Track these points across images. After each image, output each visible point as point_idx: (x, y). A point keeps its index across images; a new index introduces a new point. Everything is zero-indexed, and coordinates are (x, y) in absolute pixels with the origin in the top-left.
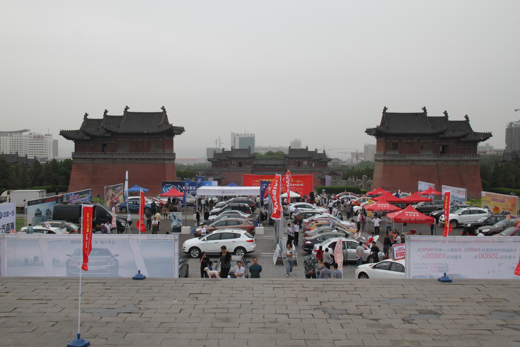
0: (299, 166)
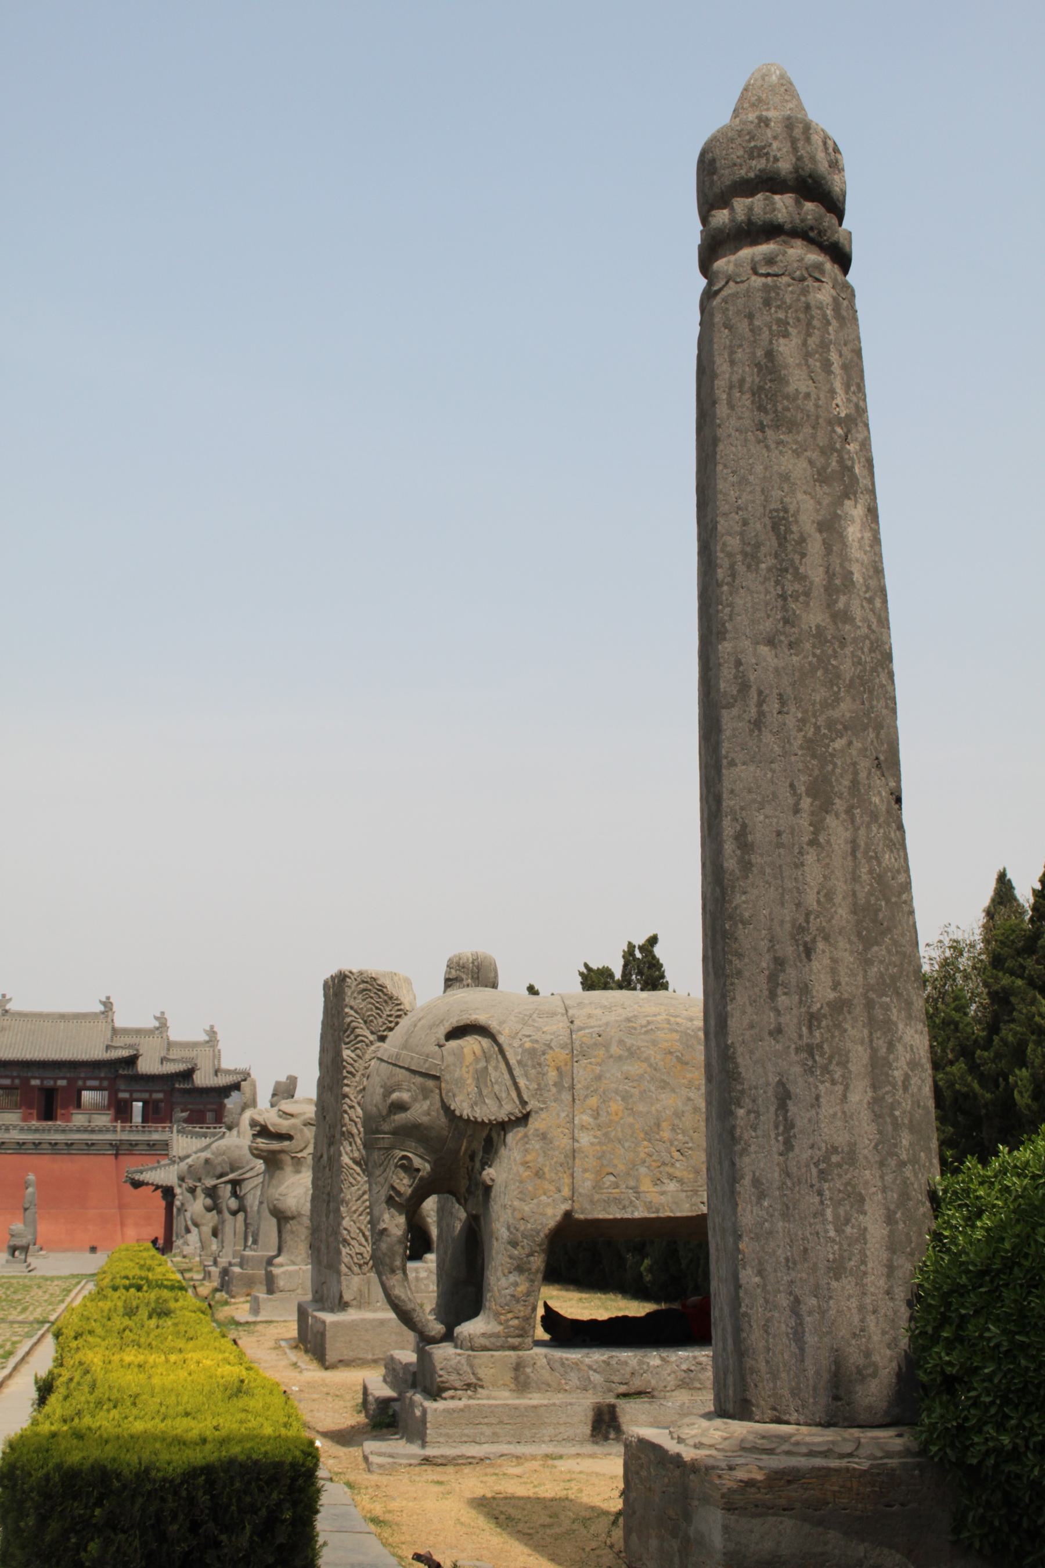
0: (48, 1114)
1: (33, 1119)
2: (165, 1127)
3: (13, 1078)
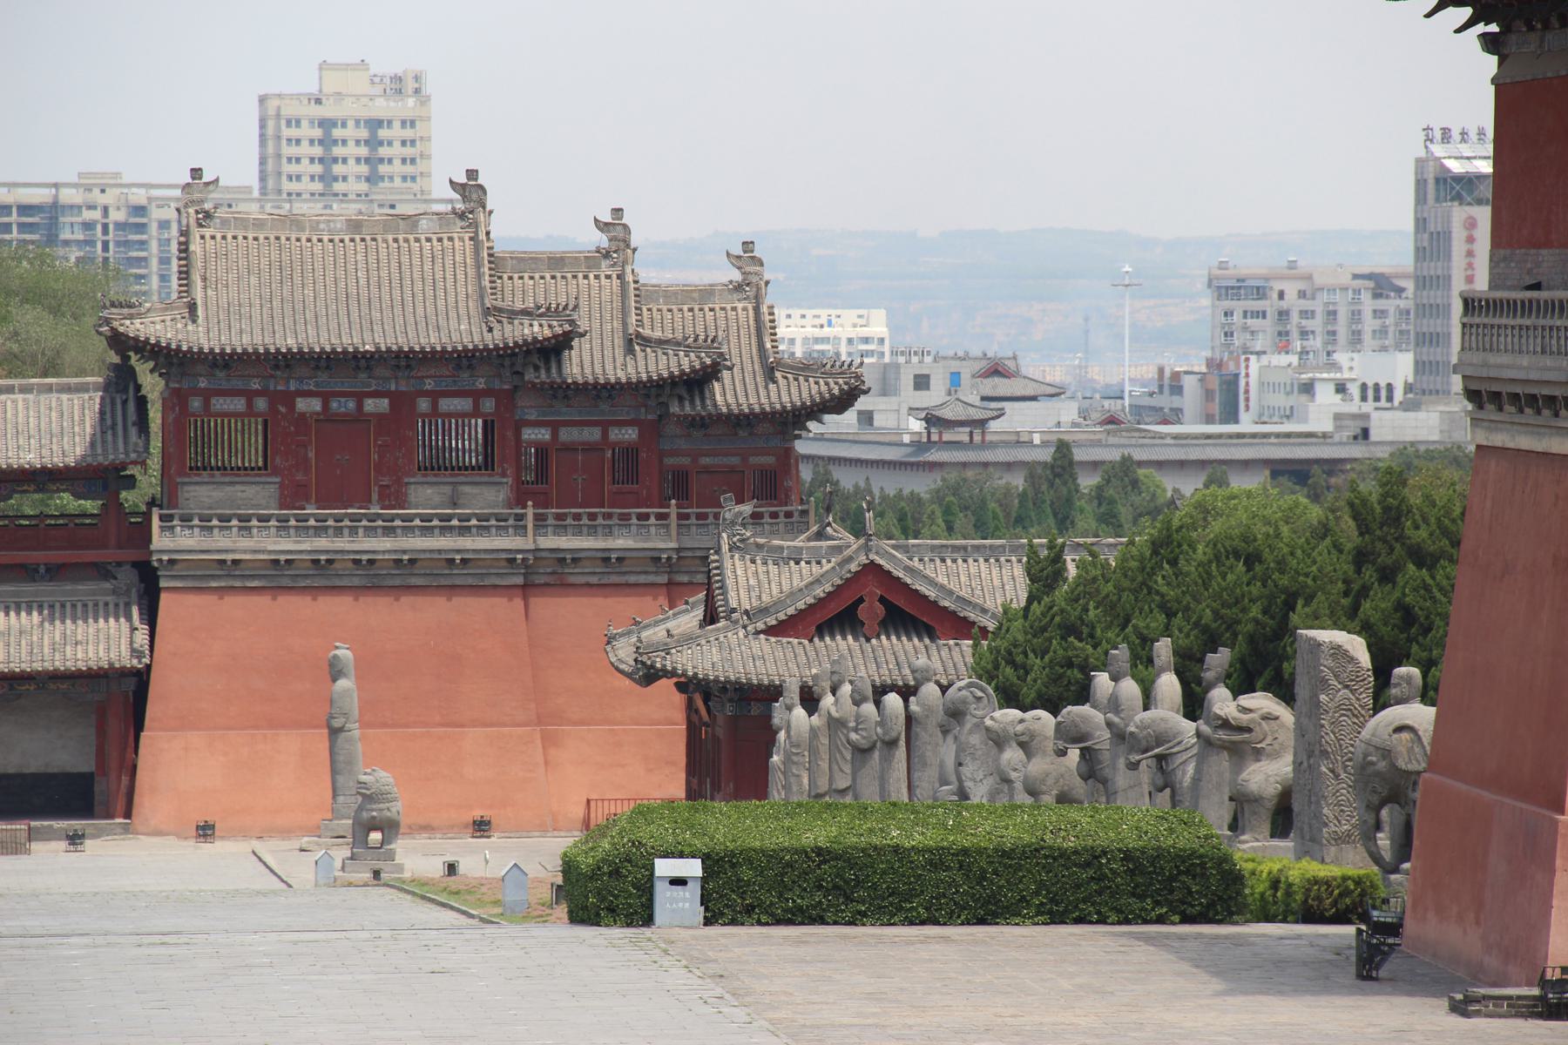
1: (308, 500)
2: (646, 517)
3: (250, 395)
